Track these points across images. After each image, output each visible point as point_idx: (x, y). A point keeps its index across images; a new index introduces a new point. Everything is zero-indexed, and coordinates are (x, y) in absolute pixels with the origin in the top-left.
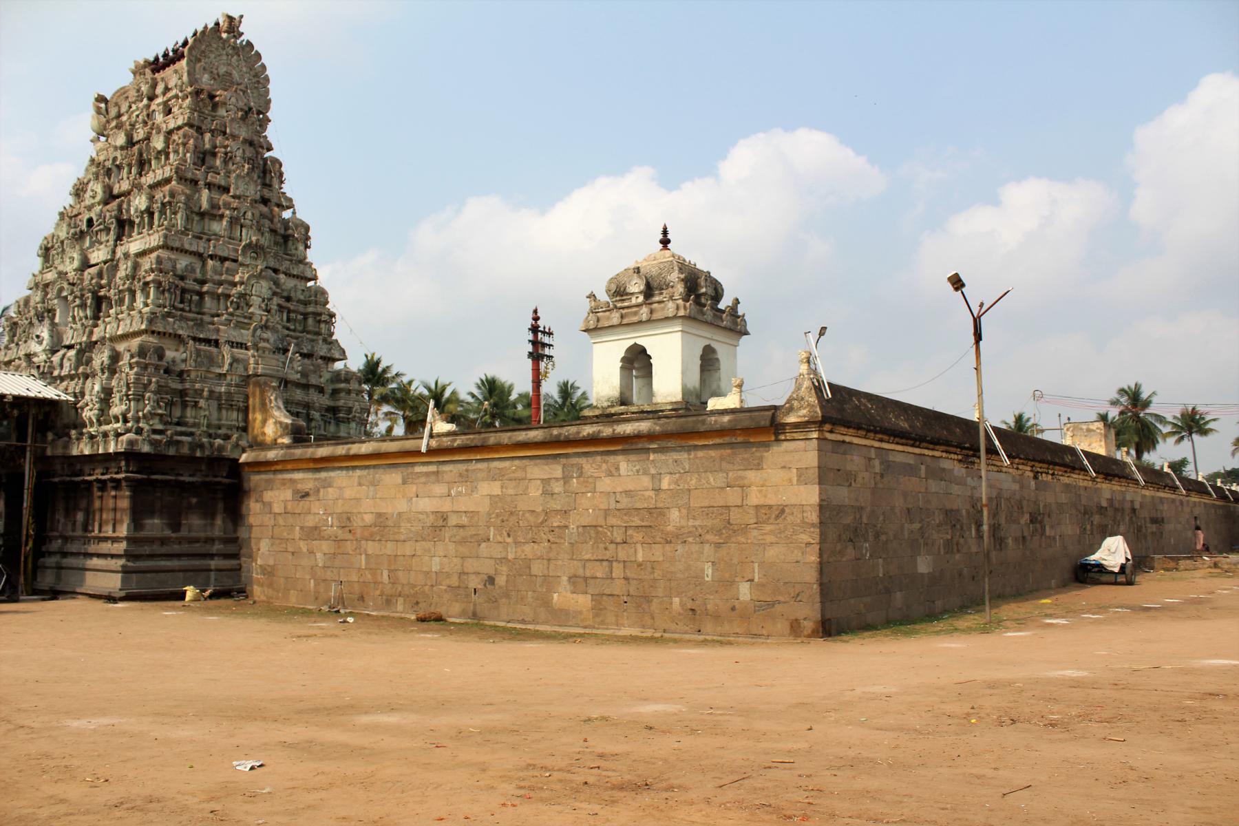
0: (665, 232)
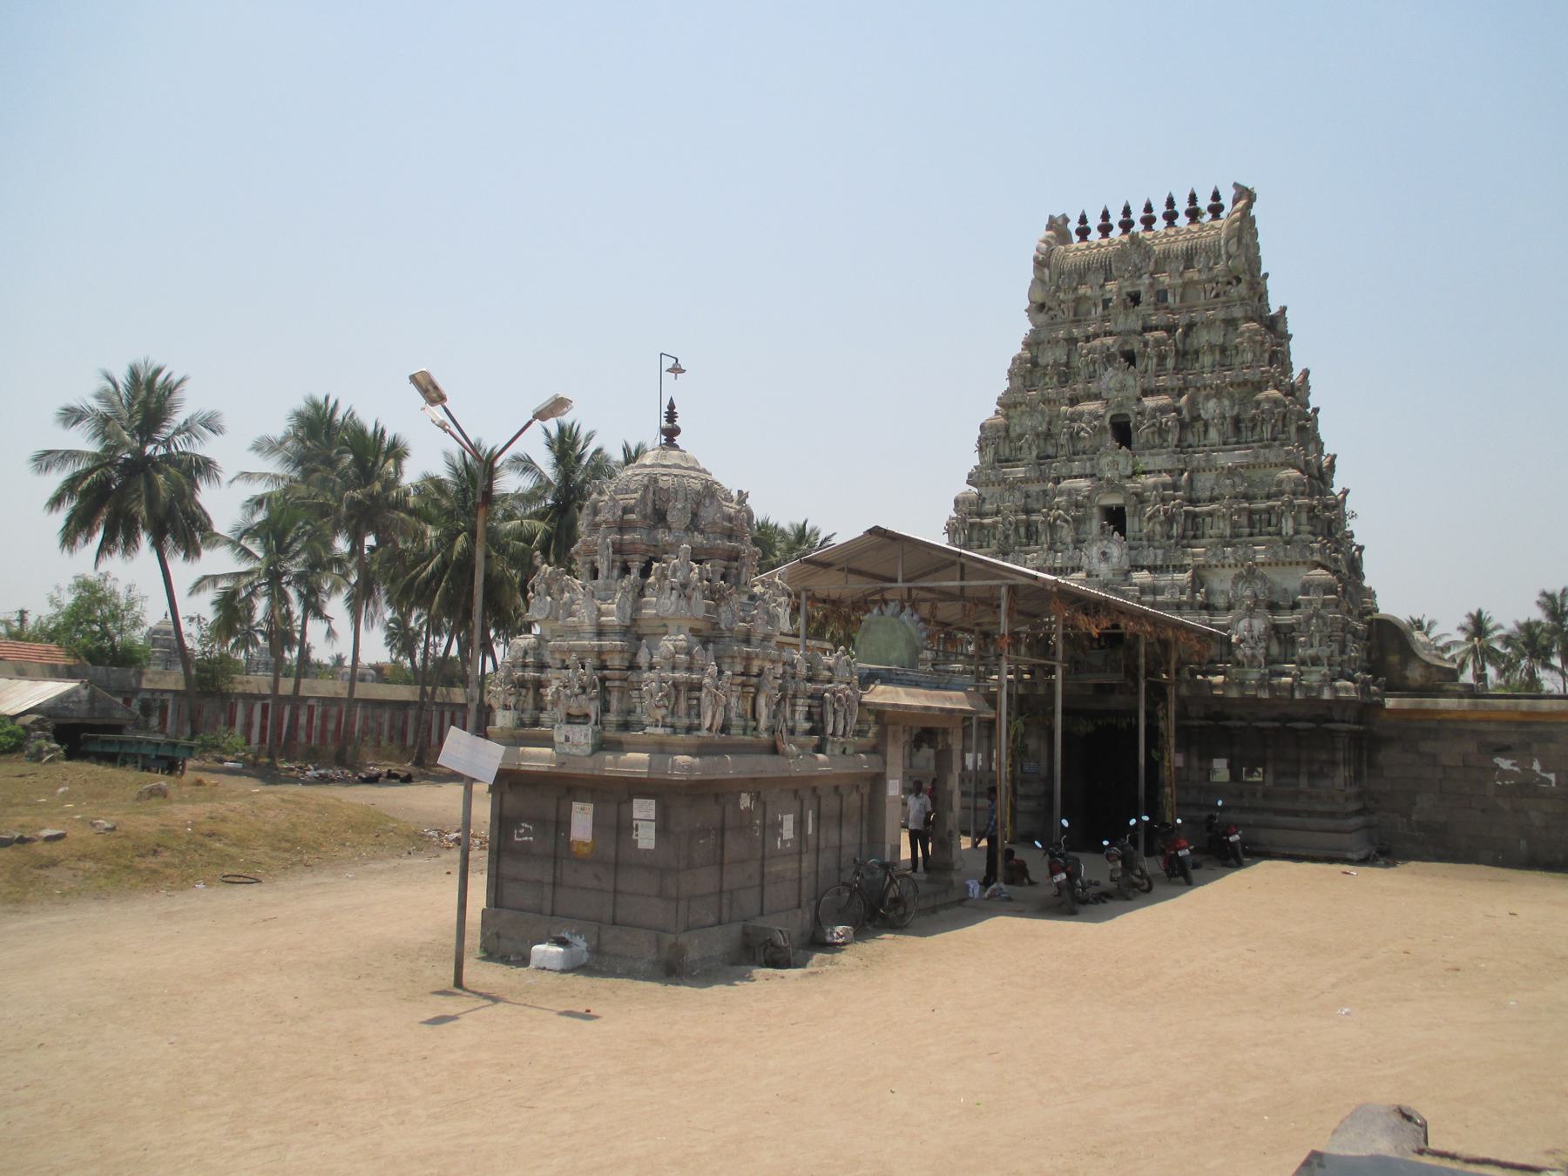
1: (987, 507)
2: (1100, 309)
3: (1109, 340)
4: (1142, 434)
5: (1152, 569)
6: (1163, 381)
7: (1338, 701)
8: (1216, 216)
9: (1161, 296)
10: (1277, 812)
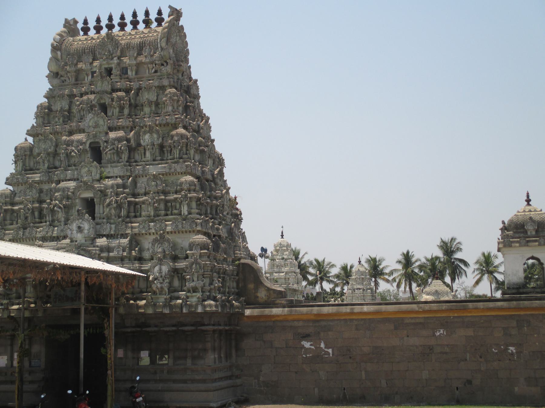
0: (528, 196)
1: (17, 199)
2: (90, 77)
3: (92, 97)
4: (107, 155)
5: (108, 236)
6: (121, 122)
7: (206, 313)
8: (159, 25)
9: (124, 71)
10: (175, 381)
